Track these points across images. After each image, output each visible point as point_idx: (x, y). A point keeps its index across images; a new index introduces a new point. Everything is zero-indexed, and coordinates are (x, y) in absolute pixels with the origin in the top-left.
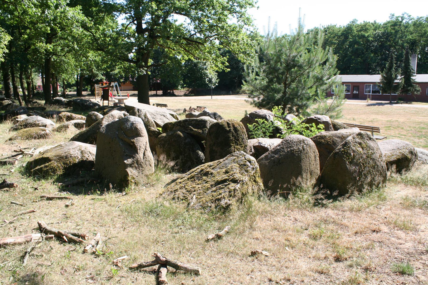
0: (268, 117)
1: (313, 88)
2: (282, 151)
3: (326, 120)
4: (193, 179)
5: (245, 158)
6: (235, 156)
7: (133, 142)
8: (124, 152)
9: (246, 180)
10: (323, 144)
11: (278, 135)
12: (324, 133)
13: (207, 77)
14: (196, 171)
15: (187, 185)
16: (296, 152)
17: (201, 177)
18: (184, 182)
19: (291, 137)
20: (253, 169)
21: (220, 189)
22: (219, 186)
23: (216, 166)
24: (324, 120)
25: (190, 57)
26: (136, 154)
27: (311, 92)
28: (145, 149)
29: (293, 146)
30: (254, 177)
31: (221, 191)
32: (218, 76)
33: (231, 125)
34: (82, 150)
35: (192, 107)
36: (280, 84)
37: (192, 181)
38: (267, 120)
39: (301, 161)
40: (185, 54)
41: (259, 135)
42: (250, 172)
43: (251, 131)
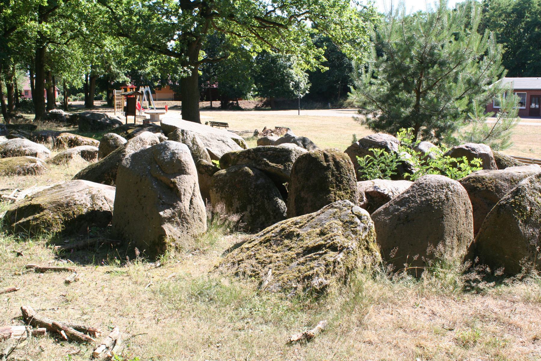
2: (413, 202)
3: (484, 152)
4: (268, 244)
5: (352, 211)
6: (335, 208)
7: (174, 183)
8: (159, 198)
9: (353, 247)
10: (480, 191)
11: (406, 174)
12: (481, 172)
13: (292, 81)
14: (273, 231)
15: (258, 253)
16: (435, 202)
18: (253, 248)
19: (427, 178)
21: (311, 261)
22: (310, 255)
24: (482, 152)
25: (266, 48)
26: (179, 202)
27: (460, 106)
29: (430, 194)
30: (367, 242)
33: (330, 159)
34: (93, 193)
35: (268, 128)
36: (409, 92)
37: (266, 247)
38: (387, 150)
39: (443, 217)
40: (258, 43)
41: (375, 174)
42: (360, 235)
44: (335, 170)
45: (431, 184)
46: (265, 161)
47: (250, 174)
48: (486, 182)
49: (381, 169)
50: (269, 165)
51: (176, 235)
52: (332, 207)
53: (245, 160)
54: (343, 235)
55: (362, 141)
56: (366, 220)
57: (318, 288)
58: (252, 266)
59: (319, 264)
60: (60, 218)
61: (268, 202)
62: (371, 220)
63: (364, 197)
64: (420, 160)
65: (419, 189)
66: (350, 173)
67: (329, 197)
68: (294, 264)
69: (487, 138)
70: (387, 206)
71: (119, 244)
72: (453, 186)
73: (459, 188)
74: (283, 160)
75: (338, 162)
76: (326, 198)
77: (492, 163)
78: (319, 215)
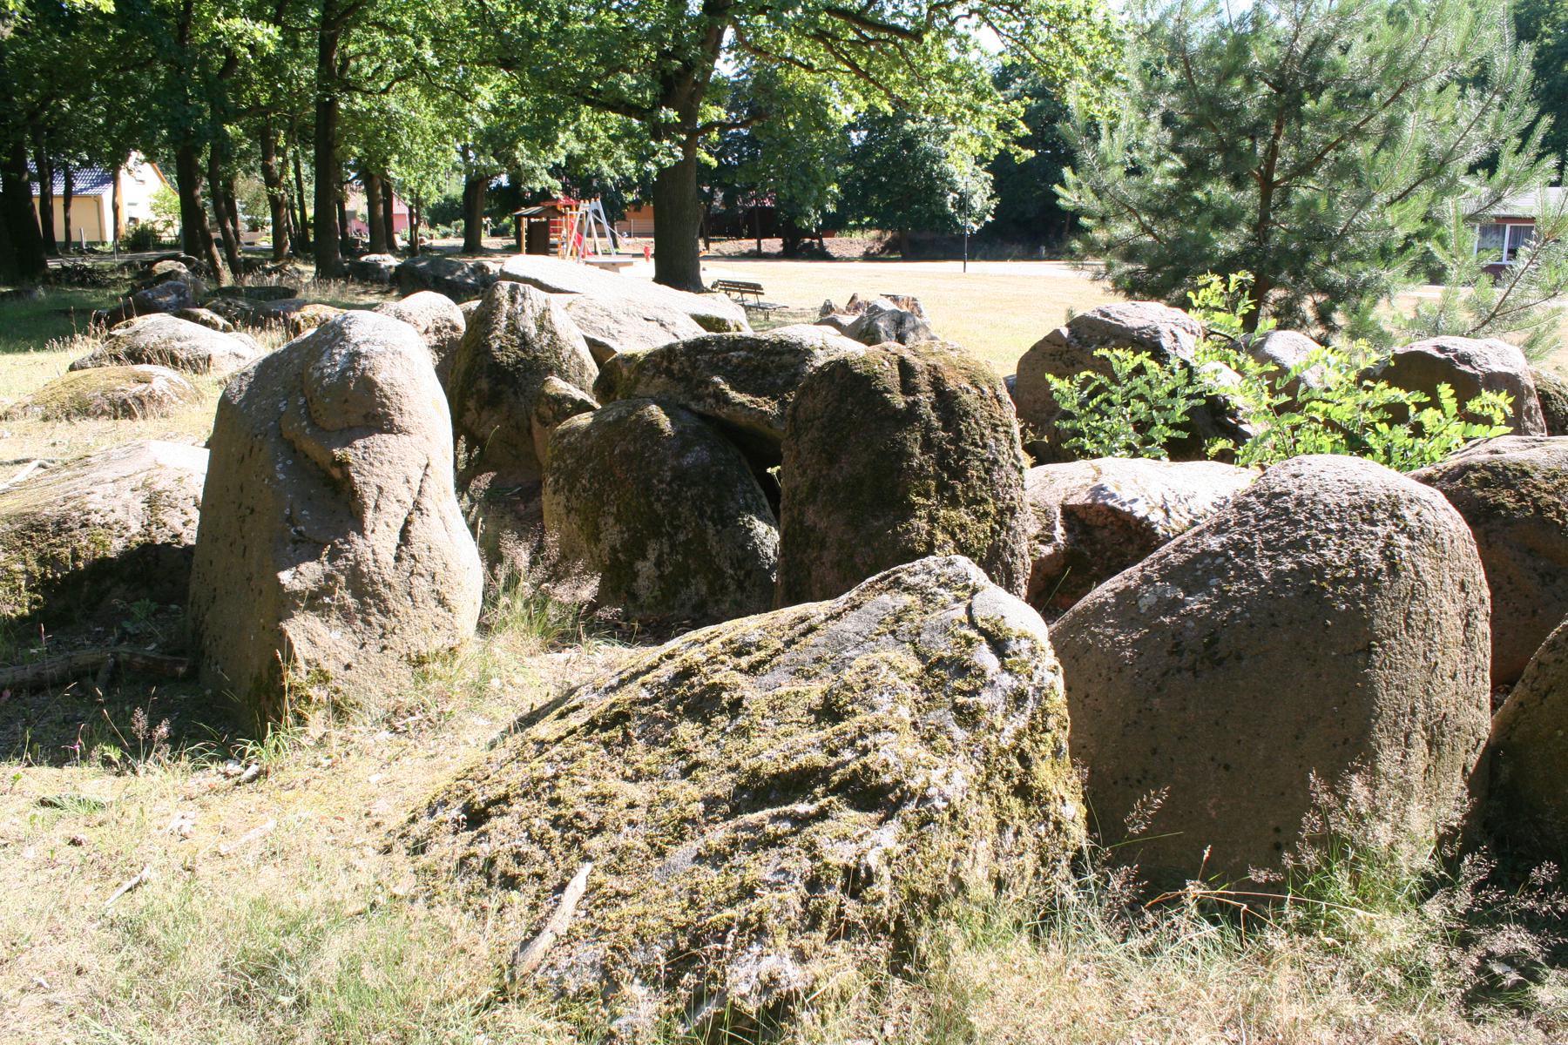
0: (1166, 343)
1: (1413, 201)
2: (1241, 574)
3: (1503, 369)
4: (617, 733)
5: (969, 609)
6: (908, 589)
7: (343, 465)
8: (290, 520)
9: (948, 791)
10: (1509, 520)
11: (1222, 444)
12: (1511, 449)
13: (953, 190)
14: (649, 678)
15: (570, 774)
16: (1336, 582)
17: (670, 725)
18: (559, 748)
19: (1305, 470)
20: (1019, 698)
21: (752, 847)
22: (751, 818)
23: (777, 652)
24: (1497, 368)
25: (877, 100)
26: (354, 536)
27: (1401, 220)
28: (417, 506)
29: (1316, 543)
30: (1024, 759)
31: (759, 868)
32: (994, 187)
33: (923, 381)
34: (159, 487)
35: (860, 299)
36: (1238, 183)
37: (606, 744)
38: (1159, 355)
39: (1369, 650)
40: (856, 88)
41: (1113, 436)
42: (992, 727)
43: (1068, 416)
44: (936, 424)
45: (1323, 496)
46: (716, 385)
47: (662, 431)
48: (1535, 486)
49: (1135, 418)
50: (727, 401)
51: (336, 658)
52: (897, 583)
53: (658, 381)
54: (914, 724)
55: (1078, 325)
56: (1025, 656)
57: (751, 1007)
58: (530, 837)
59: (783, 870)
60: (26, 572)
61: (718, 532)
62: (1051, 653)
63: (1058, 525)
64: (1273, 392)
65: (1267, 517)
66: (997, 439)
67: (907, 531)
68: (682, 854)
69: (1484, 323)
70: (1132, 583)
71: (181, 670)
72: (1416, 508)
73: (1443, 516)
74: (780, 382)
75: (953, 396)
76: (896, 534)
77: (1530, 408)
78: (837, 616)
